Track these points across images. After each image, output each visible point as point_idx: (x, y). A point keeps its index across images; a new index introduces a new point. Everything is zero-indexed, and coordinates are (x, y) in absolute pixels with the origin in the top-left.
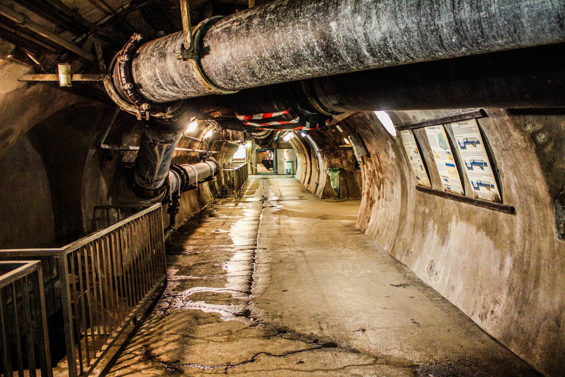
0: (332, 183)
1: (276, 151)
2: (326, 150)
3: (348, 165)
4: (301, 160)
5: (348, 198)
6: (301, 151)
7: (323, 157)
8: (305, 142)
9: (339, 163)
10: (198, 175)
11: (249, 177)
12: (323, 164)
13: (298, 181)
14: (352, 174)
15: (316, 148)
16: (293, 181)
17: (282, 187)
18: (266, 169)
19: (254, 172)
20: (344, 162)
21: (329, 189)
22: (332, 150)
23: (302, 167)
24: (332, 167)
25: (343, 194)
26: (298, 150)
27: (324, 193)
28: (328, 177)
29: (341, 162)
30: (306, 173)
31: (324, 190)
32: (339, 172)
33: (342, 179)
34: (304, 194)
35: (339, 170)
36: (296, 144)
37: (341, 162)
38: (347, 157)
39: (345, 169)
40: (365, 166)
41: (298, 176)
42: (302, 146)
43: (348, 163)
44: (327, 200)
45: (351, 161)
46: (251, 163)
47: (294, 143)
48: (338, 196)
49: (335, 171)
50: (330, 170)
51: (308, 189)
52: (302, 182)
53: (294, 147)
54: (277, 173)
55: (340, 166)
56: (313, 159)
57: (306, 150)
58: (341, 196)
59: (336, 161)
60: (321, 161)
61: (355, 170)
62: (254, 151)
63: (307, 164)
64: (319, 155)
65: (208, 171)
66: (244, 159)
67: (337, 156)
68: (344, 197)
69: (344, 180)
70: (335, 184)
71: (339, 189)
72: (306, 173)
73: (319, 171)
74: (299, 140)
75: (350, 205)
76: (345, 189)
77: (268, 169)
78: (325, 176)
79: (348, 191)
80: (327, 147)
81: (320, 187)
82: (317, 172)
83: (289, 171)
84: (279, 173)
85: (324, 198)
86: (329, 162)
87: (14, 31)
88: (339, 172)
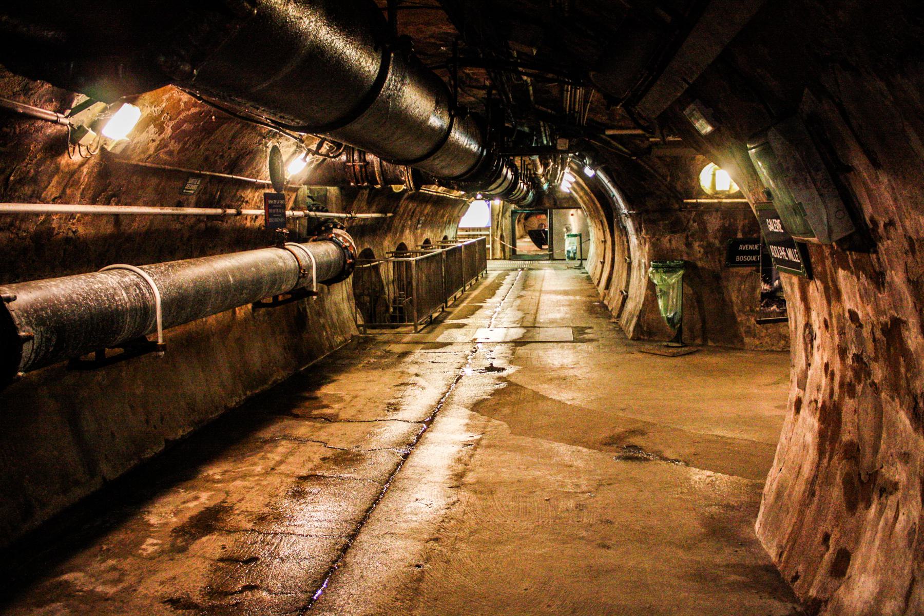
0: (661, 303)
1: (551, 214)
2: (647, 211)
3: (706, 253)
4: (595, 233)
5: (704, 344)
6: (593, 214)
7: (638, 231)
8: (595, 187)
9: (683, 248)
10: (163, 303)
11: (490, 264)
12: (638, 249)
13: (589, 279)
14: (717, 278)
15: (623, 208)
16: (577, 277)
17: (555, 290)
18: (536, 248)
19: (508, 254)
20: (696, 245)
21: (652, 317)
22: (664, 211)
23: (597, 249)
24: (661, 260)
25: (691, 330)
26: (590, 211)
27: (638, 326)
28: (651, 286)
29: (689, 245)
30: (603, 263)
31: (639, 317)
32: (681, 272)
33: (689, 291)
34: (592, 322)
35: (681, 267)
36: (585, 198)
37: (689, 245)
38: (704, 230)
39: (699, 264)
40: (815, 289)
41: (590, 266)
42: (594, 203)
43: (709, 249)
44: (648, 347)
45: (717, 242)
46: (502, 237)
47: (581, 197)
48: (678, 338)
49: (670, 270)
50: (656, 268)
51: (606, 302)
52: (596, 282)
53: (582, 205)
54: (552, 258)
55: (685, 258)
56: (616, 233)
57: (602, 213)
58: (686, 335)
59: (673, 242)
60: (634, 240)
61: (727, 266)
62: (508, 214)
63: (605, 242)
64: (629, 225)
65: (289, 271)
66: (487, 229)
67: (676, 227)
68: (693, 338)
69: (695, 293)
70: (667, 308)
71: (681, 320)
72: (603, 263)
73: (630, 264)
74: (586, 188)
75: (710, 372)
76: (697, 316)
77: (540, 247)
78: (644, 282)
79: (704, 322)
80: (650, 204)
81: (630, 306)
82: (626, 266)
83: (572, 255)
84: (555, 256)
85: (638, 339)
86: (654, 245)
87: (436, 121)
88: (681, 272)
